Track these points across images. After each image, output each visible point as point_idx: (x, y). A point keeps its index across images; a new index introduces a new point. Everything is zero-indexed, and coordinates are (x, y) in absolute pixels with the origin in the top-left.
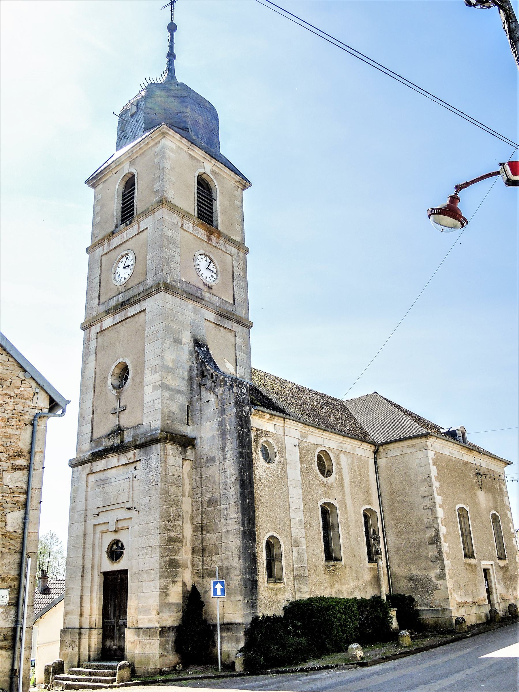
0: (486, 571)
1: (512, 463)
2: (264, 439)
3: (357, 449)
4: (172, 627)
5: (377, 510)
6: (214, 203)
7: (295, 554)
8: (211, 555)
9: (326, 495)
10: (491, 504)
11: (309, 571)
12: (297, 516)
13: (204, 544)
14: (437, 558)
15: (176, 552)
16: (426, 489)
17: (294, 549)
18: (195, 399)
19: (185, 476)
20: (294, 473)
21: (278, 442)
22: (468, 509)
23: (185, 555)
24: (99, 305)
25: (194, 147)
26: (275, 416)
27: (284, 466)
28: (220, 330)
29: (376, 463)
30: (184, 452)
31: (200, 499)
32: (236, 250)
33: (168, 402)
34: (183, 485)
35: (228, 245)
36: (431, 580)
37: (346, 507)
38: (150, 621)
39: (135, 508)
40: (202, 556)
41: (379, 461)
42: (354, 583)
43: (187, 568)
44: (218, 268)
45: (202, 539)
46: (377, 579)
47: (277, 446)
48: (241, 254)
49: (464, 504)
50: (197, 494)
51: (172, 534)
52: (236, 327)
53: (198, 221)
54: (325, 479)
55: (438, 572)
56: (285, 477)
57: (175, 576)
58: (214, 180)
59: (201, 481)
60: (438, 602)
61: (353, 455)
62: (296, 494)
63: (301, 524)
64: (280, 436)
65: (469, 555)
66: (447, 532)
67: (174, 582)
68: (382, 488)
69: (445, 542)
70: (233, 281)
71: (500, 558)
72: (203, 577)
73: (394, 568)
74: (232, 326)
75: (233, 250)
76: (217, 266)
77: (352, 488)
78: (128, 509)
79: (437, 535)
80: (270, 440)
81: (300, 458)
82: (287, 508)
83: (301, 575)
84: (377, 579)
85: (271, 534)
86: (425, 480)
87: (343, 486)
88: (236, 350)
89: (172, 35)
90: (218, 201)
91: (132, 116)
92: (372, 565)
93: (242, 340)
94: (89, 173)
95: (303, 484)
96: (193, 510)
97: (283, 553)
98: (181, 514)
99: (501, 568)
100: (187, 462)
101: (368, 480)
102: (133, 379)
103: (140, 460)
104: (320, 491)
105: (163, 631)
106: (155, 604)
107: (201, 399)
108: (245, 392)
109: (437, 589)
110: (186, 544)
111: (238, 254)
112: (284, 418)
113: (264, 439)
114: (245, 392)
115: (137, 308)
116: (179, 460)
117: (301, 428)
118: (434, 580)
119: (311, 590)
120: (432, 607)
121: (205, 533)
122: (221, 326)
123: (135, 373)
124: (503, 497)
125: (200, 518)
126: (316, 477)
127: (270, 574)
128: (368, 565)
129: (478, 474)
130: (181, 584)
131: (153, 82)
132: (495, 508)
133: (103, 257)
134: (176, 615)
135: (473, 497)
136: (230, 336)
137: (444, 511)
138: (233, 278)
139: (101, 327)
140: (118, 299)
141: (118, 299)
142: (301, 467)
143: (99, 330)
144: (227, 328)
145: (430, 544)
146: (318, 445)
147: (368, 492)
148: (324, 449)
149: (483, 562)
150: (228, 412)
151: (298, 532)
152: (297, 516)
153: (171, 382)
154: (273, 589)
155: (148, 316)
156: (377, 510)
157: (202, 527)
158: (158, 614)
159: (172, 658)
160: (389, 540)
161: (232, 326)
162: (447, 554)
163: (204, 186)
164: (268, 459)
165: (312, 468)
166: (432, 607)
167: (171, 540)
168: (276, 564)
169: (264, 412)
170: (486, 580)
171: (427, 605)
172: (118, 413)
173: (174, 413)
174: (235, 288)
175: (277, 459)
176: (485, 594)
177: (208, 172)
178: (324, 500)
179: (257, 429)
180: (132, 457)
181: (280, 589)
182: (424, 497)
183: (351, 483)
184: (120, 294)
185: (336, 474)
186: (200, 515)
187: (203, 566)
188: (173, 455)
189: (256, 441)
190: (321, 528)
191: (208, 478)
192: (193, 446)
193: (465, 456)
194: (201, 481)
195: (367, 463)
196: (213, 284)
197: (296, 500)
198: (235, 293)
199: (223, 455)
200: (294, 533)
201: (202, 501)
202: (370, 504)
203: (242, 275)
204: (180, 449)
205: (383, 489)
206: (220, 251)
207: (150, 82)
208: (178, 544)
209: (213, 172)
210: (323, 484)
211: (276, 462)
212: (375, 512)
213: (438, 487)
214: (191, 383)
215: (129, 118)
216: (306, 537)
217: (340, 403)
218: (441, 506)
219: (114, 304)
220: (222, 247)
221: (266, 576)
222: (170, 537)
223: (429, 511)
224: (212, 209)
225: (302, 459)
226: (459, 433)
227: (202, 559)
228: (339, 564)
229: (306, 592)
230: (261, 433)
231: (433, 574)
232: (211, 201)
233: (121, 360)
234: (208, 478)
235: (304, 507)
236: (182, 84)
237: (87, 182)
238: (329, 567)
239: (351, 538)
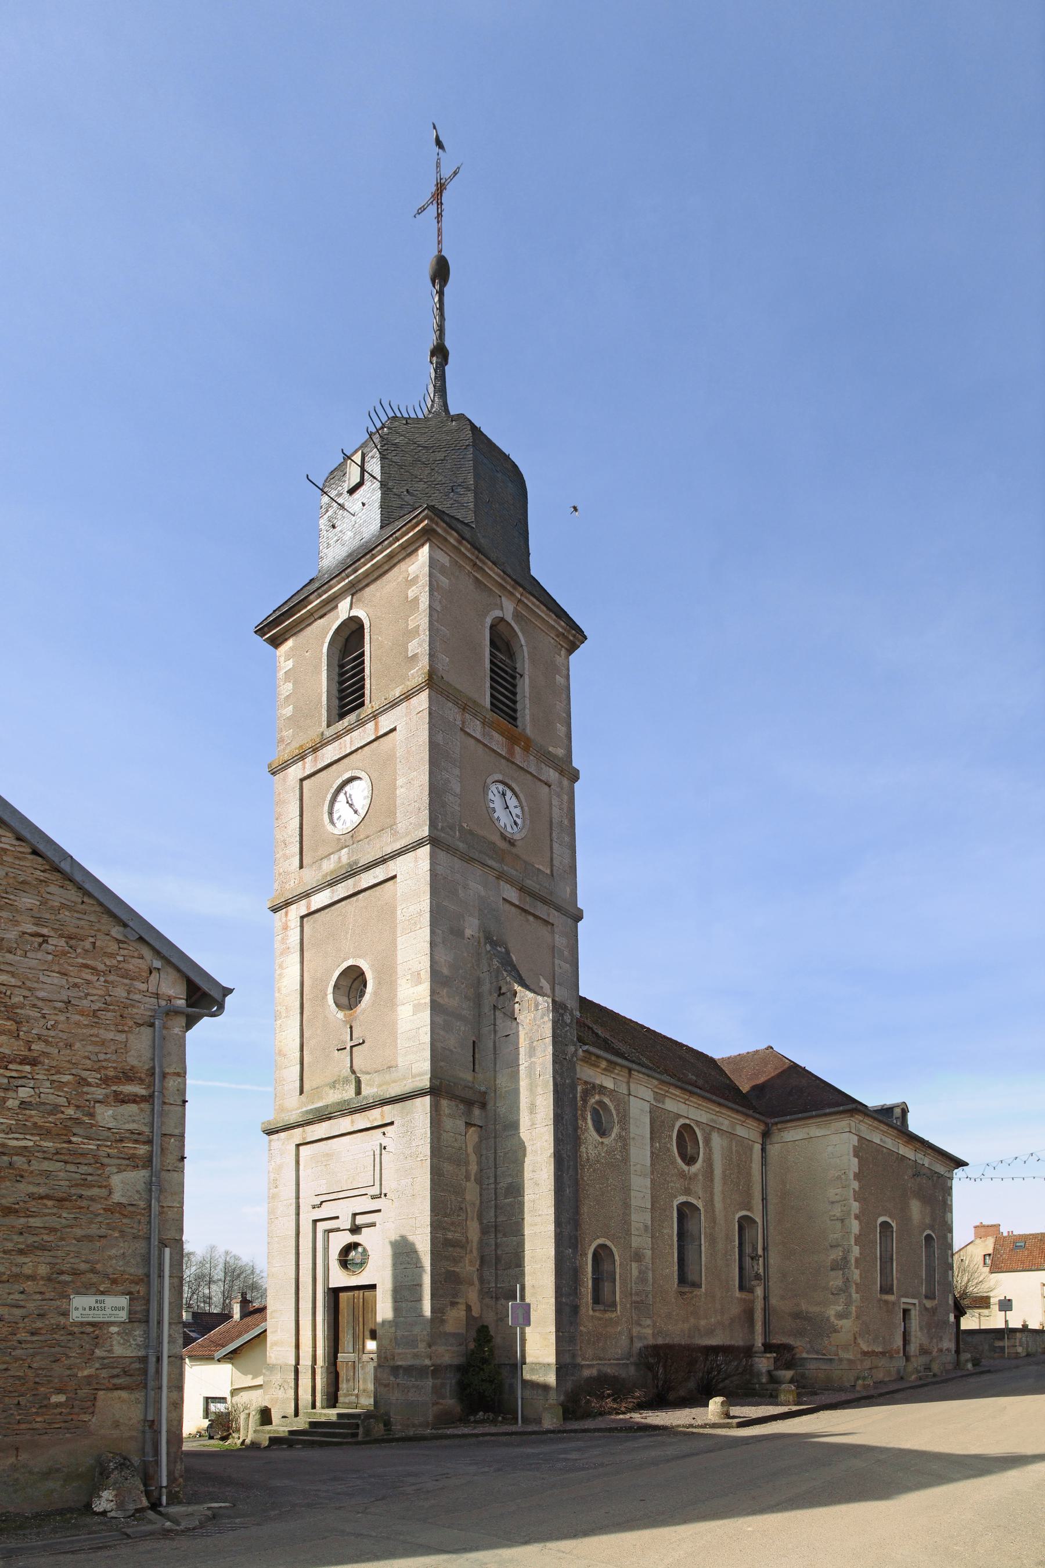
0: (906, 1312)
1: (966, 1164)
2: (597, 1097)
3: (738, 1127)
4: (451, 1365)
5: (759, 1220)
6: (519, 682)
7: (635, 1273)
8: (510, 1268)
9: (687, 1191)
10: (927, 1221)
11: (653, 1297)
12: (640, 1218)
13: (499, 1252)
14: (841, 1290)
15: (456, 1261)
16: (838, 1191)
17: (634, 1265)
18: (485, 1030)
19: (470, 1150)
20: (641, 1154)
21: (618, 1105)
22: (894, 1225)
23: (468, 1267)
24: (301, 867)
25: (484, 563)
26: (616, 1064)
27: (624, 1141)
28: (528, 920)
29: (763, 1150)
30: (469, 1113)
31: (493, 1186)
32: (557, 774)
33: (442, 1033)
34: (467, 1163)
35: (543, 765)
36: (828, 1319)
37: (714, 1211)
38: (416, 1356)
39: (385, 1195)
40: (496, 1269)
41: (768, 1147)
42: (710, 1320)
43: (473, 1284)
44: (526, 808)
45: (496, 1244)
46: (749, 1315)
47: (617, 1110)
48: (566, 782)
49: (890, 1217)
50: (488, 1178)
51: (450, 1235)
52: (554, 916)
53: (490, 716)
54: (685, 1168)
55: (840, 1308)
56: (626, 1160)
57: (455, 1296)
58: (520, 634)
59: (495, 1159)
60: (834, 1349)
61: (731, 1135)
62: (640, 1186)
63: (646, 1230)
64: (622, 1096)
65: (886, 1289)
66: (861, 1254)
67: (453, 1304)
68: (769, 1189)
69: (856, 1268)
70: (551, 834)
71: (926, 1297)
72: (497, 1299)
73: (774, 1301)
74: (549, 915)
75: (552, 775)
76: (525, 804)
77: (724, 1184)
78: (373, 1197)
79: (845, 1258)
80: (606, 1100)
81: (651, 1133)
82: (626, 1206)
83: (642, 1302)
84: (749, 1315)
85: (600, 1241)
86: (839, 1178)
87: (712, 1180)
88: (554, 957)
89: (441, 293)
90: (526, 677)
91: (351, 491)
92: (744, 1295)
93: (564, 941)
94: (264, 611)
95: (652, 1173)
96: (481, 1202)
97: (618, 1270)
98: (463, 1206)
99: (926, 1309)
100: (473, 1128)
101: (749, 1174)
102: (375, 993)
103: (392, 1123)
104: (677, 1184)
105: (437, 1371)
106: (425, 1333)
107: (495, 1031)
108: (568, 1021)
109: (836, 1331)
110: (471, 1251)
111: (560, 783)
112: (630, 1070)
113: (597, 1097)
114: (568, 1021)
115: (378, 874)
116: (461, 1124)
117: (656, 1087)
118: (832, 1319)
119: (654, 1323)
120: (824, 1355)
121: (499, 1235)
122: (530, 913)
123: (379, 983)
124: (945, 1212)
125: (492, 1214)
126: (673, 1162)
127: (597, 1300)
128: (738, 1294)
129: (916, 1175)
130: (463, 1307)
131: (399, 415)
132: (932, 1228)
133: (305, 783)
134: (456, 1349)
135: (905, 1209)
136: (544, 931)
137: (860, 1224)
138: (551, 829)
139: (308, 907)
140: (340, 858)
141: (340, 858)
142: (652, 1146)
143: (304, 912)
144: (540, 918)
145: (832, 1269)
146: (679, 1116)
147: (748, 1193)
148: (687, 1122)
149: (904, 1300)
150: (539, 1053)
151: (640, 1241)
152: (640, 1218)
153: (446, 1000)
154: (600, 1319)
155: (400, 886)
156: (759, 1220)
157: (496, 1226)
158: (430, 1346)
159: (450, 1402)
160: (771, 1261)
161: (549, 915)
162: (856, 1284)
163: (502, 642)
164: (602, 1131)
165: (668, 1150)
166: (824, 1355)
167: (448, 1243)
168: (606, 1286)
169: (598, 1057)
170: (904, 1321)
171: (817, 1353)
172: (348, 1048)
173: (451, 1051)
174: (556, 846)
175: (616, 1130)
176: (900, 1343)
177: (509, 618)
178: (682, 1199)
179: (586, 1083)
180: (379, 1117)
181: (611, 1319)
182: (833, 1203)
183: (724, 1176)
184: (342, 848)
185: (704, 1161)
186: (493, 1210)
187: (496, 1283)
188: (450, 1116)
189: (585, 1100)
190: (675, 1239)
191: (506, 1154)
192: (483, 1106)
193: (901, 1147)
194: (495, 1159)
195: (751, 1149)
196: (517, 837)
197: (642, 1195)
198: (555, 856)
199: (531, 1120)
200: (635, 1242)
201: (496, 1189)
202: (748, 1210)
203: (566, 822)
204: (462, 1106)
205: (770, 1191)
206: (529, 777)
207: (391, 414)
208: (458, 1250)
209: (517, 615)
210: (682, 1175)
211: (613, 1135)
212: (755, 1222)
213: (857, 1189)
214: (478, 1000)
215: (346, 495)
216: (653, 1249)
217: (710, 1061)
218: (857, 1217)
219: (332, 867)
220: (532, 770)
221: (590, 1301)
222: (446, 1239)
223: (839, 1225)
224: (515, 694)
225: (655, 1134)
226: (898, 1112)
227: (496, 1274)
228: (696, 1292)
229: (648, 1326)
230: (593, 1088)
231: (831, 1312)
232: (514, 678)
233: (350, 962)
234: (506, 1154)
235: (652, 1205)
236: (461, 417)
237: (261, 631)
238: (682, 1294)
239: (717, 1255)
